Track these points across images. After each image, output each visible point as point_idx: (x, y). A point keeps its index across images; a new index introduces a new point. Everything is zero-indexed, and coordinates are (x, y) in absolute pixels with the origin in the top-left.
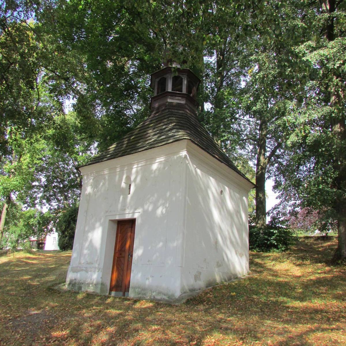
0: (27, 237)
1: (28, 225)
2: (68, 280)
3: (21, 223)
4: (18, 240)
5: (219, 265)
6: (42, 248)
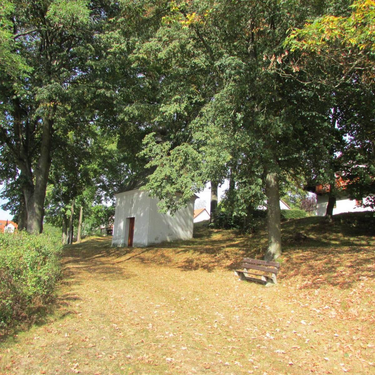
0: (98, 226)
1: (97, 217)
2: (112, 243)
3: (93, 216)
4: (91, 229)
5: (169, 235)
6: (111, 234)
